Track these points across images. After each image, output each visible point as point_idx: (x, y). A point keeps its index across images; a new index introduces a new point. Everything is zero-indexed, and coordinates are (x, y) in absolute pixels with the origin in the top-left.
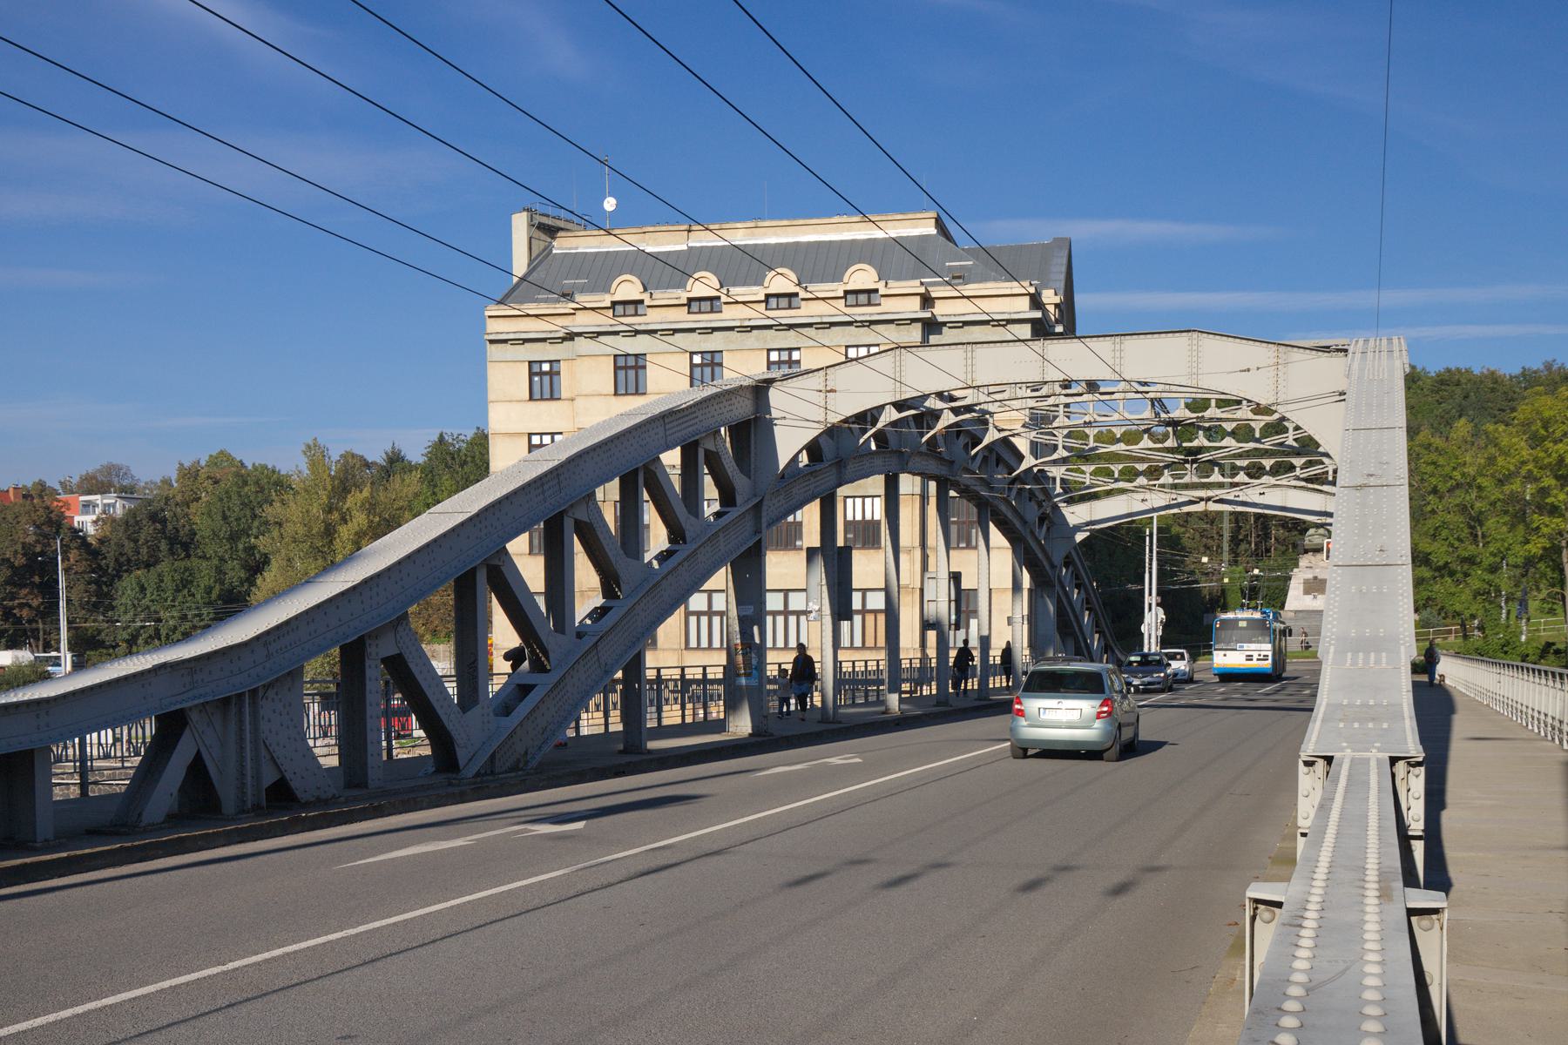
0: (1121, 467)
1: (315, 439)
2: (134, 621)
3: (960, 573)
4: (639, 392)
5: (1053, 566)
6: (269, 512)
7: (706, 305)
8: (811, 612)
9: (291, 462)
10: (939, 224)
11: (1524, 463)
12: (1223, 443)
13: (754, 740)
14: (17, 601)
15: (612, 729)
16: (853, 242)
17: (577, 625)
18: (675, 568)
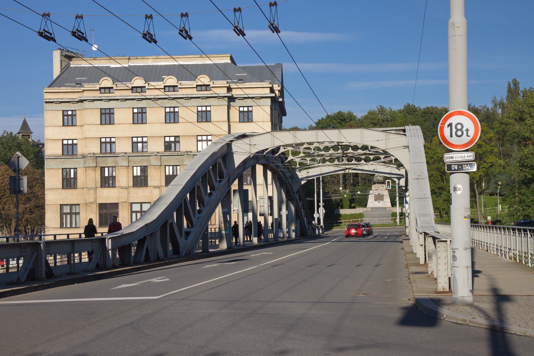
7: (139, 90)
10: (232, 59)
13: (228, 250)
15: (83, 261)
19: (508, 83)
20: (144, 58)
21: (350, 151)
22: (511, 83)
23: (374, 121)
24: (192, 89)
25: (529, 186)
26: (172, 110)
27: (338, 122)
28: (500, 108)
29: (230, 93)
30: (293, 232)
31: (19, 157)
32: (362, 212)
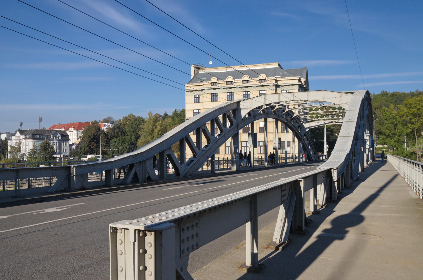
0: (315, 115)
1: (150, 111)
2: (114, 149)
3: (280, 138)
4: (216, 101)
5: (302, 136)
6: (141, 126)
8: (249, 146)
9: (145, 116)
10: (279, 65)
11: (406, 113)
12: (336, 111)
13: (236, 171)
14: (91, 145)
15: (209, 169)
16: (261, 69)
17: (202, 148)
18: (221, 138)
20: (234, 67)
26: (247, 93)
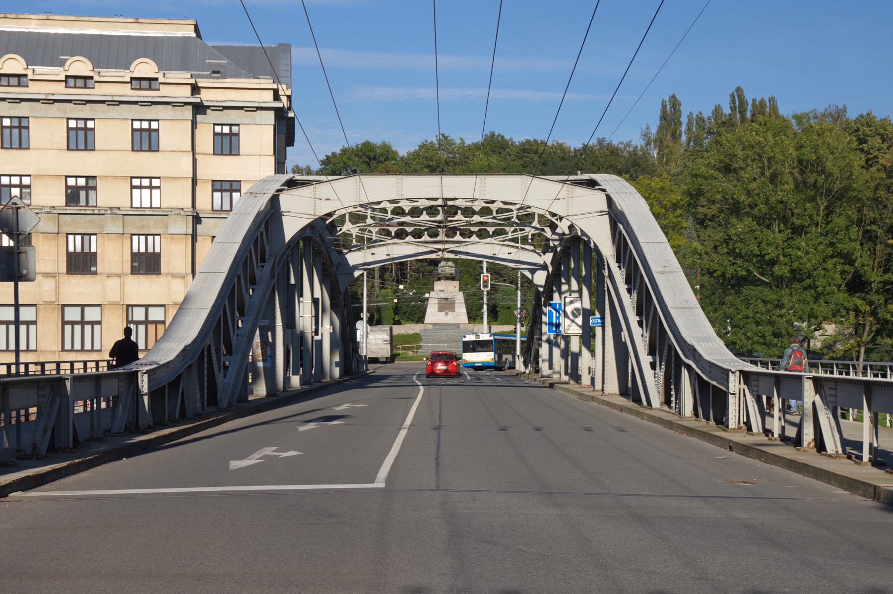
19: (663, 103)
21: (459, 216)
22: (668, 103)
23: (431, 163)
24: (123, 84)
25: (739, 290)
26: (81, 124)
27: (364, 162)
28: (655, 147)
29: (196, 96)
30: (336, 366)
31: (19, 208)
32: (419, 332)
